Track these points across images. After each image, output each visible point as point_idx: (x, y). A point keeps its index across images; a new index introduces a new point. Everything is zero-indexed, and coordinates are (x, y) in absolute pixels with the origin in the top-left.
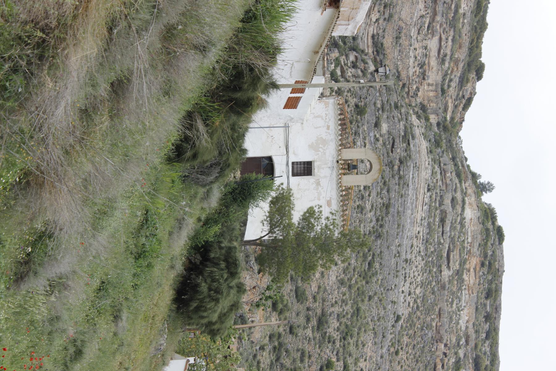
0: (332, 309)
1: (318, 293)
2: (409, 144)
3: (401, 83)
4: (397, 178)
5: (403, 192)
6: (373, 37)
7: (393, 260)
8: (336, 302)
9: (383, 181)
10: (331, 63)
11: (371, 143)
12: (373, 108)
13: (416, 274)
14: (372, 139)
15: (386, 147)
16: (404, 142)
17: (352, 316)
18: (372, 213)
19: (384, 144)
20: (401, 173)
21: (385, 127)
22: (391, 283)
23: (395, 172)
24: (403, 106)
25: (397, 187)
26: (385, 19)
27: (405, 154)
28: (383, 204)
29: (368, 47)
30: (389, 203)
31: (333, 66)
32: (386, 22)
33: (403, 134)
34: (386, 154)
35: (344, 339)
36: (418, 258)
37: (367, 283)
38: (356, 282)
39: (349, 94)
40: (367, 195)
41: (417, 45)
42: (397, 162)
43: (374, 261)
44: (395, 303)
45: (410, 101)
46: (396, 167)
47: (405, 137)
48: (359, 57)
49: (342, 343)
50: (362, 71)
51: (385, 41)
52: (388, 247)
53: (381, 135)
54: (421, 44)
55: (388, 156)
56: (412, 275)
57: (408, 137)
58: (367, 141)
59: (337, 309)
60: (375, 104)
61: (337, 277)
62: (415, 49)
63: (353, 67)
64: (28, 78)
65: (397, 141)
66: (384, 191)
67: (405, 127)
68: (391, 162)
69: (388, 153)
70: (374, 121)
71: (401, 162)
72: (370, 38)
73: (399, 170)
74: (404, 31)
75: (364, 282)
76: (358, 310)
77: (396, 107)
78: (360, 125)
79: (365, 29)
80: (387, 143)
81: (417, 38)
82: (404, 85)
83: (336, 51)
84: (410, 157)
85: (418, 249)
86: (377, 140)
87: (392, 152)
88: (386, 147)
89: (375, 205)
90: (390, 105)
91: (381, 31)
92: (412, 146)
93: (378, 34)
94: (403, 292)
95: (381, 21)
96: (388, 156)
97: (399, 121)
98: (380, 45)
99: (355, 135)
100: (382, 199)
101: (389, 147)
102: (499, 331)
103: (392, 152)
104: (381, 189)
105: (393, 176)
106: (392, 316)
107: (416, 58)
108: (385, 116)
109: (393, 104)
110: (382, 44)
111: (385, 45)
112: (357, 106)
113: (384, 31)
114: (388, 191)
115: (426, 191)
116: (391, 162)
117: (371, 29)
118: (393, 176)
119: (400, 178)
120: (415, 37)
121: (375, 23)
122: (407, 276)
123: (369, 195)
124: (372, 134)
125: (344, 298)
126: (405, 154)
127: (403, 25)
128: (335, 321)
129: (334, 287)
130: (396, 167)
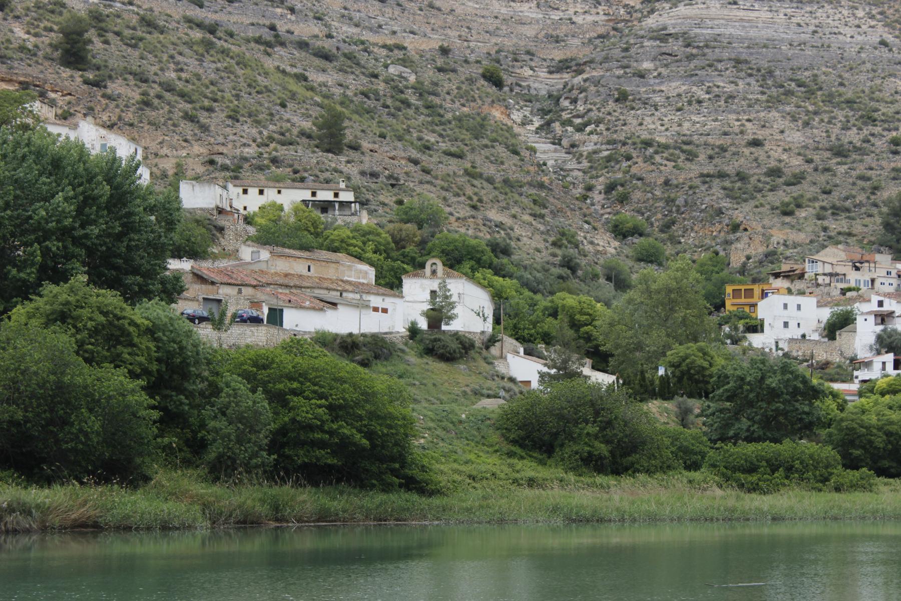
0: (833, 138)
1: (805, 156)
2: (670, 34)
3: (612, 33)
4: (706, 50)
5: (726, 41)
6: (551, 72)
7: (807, 52)
8: (827, 131)
9: (707, 68)
10: (567, 130)
11: (662, 82)
12: (622, 80)
13: (838, 16)
14: (657, 81)
15: (669, 64)
16: (666, 41)
17: (852, 110)
18: (740, 83)
19: (666, 66)
20: (701, 44)
21: (647, 65)
22: (834, 55)
23: (700, 52)
24: (627, 42)
25: (716, 50)
26: (531, 60)
27: (681, 39)
28: (734, 67)
29: (561, 78)
30: (734, 60)
31: (570, 129)
32: (534, 58)
33: (658, 42)
34: (678, 64)
35: (875, 120)
36: (818, 14)
37: (821, 89)
38: (814, 104)
39: (603, 110)
40: (716, 89)
41: (571, 11)
42: (688, 50)
43: (798, 80)
44: (862, 48)
45: (636, 19)
46: (694, 51)
47: (662, 40)
48: (565, 95)
49: (879, 124)
50: (581, 93)
51: (557, 59)
52: (789, 59)
53: (655, 70)
54: (571, 6)
55: (681, 61)
56: (836, 23)
57: (661, 35)
58: (658, 88)
59: (836, 131)
60: (619, 77)
61: (798, 130)
62: (576, 13)
63: (576, 102)
64: (729, 472)
65: (664, 50)
66: (720, 66)
67: (651, 38)
68: (687, 57)
69: (677, 61)
70: (638, 79)
71: (688, 46)
72: (551, 76)
73: (698, 47)
74: (550, 31)
75: (819, 93)
76: (848, 102)
77: (626, 50)
78: (638, 97)
79: (541, 82)
80: (665, 62)
81: (563, 11)
82: (614, 29)
83: (553, 125)
84: (685, 33)
85: (807, 15)
86: (659, 74)
87: (676, 56)
88: (669, 64)
89: (731, 79)
90: (623, 57)
91: (544, 63)
92: (673, 31)
93: (548, 67)
94: (852, 37)
95: (533, 64)
96: (681, 61)
97: (642, 47)
98: (561, 64)
99: (646, 104)
100: (727, 69)
101: (670, 59)
102: (330, 334)
103: (676, 56)
104: (716, 70)
105: (704, 55)
106: (877, 52)
107: (586, 12)
108: (635, 64)
109: (623, 54)
110: (560, 61)
111: (562, 57)
112: (617, 100)
113: (545, 60)
114: (720, 61)
115: (735, 7)
116: (687, 57)
117: (542, 74)
118: (704, 55)
119: (707, 46)
120: (561, 14)
121: (534, 71)
122: (836, 30)
123: (718, 87)
124: (652, 81)
125: (826, 120)
126: (681, 39)
127: (543, 33)
128: (848, 133)
129: (808, 134)
130: (694, 51)
